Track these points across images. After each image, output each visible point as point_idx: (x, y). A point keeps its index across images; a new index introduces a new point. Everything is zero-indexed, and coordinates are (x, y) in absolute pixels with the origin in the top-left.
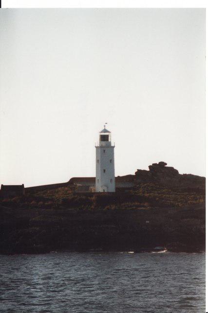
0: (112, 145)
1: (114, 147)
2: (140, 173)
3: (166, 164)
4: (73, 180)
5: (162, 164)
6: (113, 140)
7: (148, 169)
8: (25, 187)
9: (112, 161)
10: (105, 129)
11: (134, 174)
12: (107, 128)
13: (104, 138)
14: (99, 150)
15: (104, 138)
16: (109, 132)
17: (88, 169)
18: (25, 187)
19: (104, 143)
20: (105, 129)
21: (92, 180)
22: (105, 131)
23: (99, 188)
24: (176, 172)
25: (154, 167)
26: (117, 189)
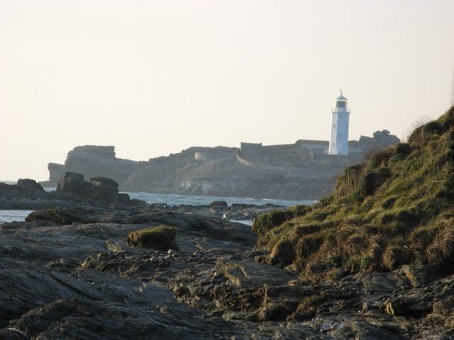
0: (348, 111)
1: (349, 113)
2: (115, 154)
3: (389, 132)
4: (300, 143)
5: (386, 133)
6: (349, 106)
7: (372, 136)
8: (117, 156)
9: (347, 126)
10: (342, 96)
11: (148, 161)
12: (344, 95)
13: (342, 104)
14: (337, 115)
15: (342, 104)
16: (344, 99)
17: (321, 130)
18: (117, 156)
19: (341, 110)
20: (342, 96)
21: (326, 143)
22: (342, 97)
23: (332, 150)
24: (35, 181)
25: (377, 134)
26: (349, 153)
